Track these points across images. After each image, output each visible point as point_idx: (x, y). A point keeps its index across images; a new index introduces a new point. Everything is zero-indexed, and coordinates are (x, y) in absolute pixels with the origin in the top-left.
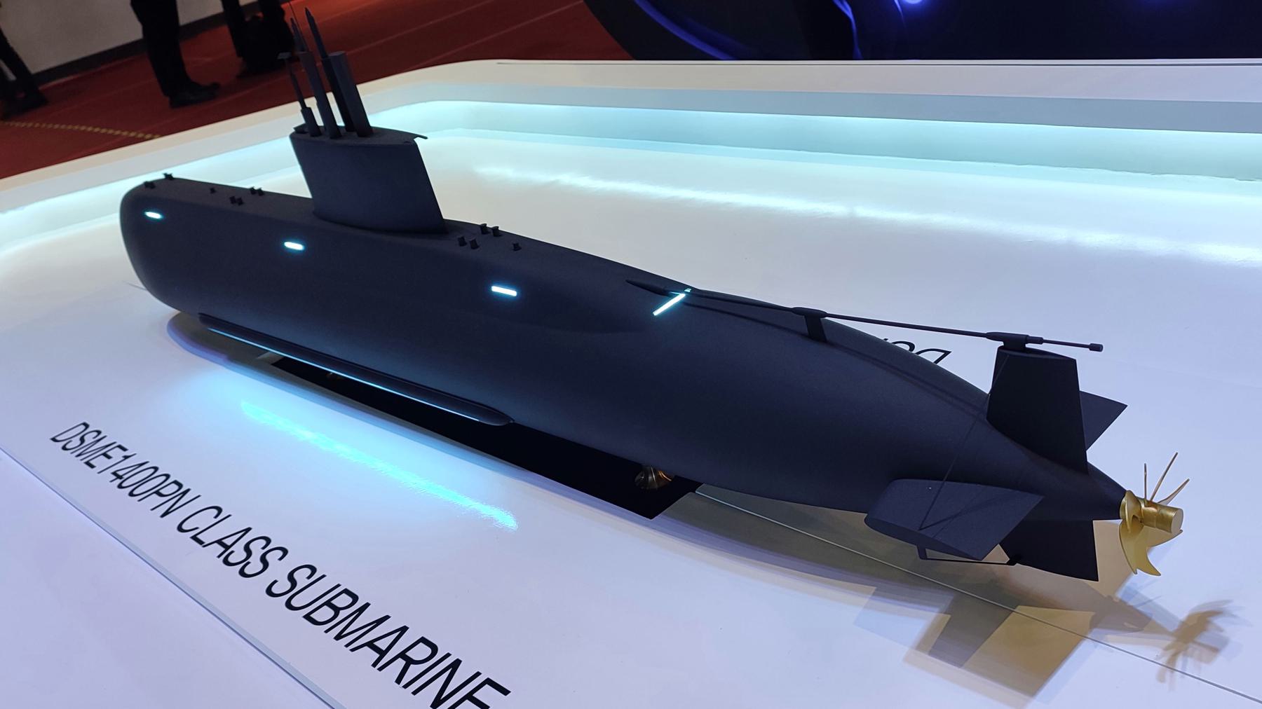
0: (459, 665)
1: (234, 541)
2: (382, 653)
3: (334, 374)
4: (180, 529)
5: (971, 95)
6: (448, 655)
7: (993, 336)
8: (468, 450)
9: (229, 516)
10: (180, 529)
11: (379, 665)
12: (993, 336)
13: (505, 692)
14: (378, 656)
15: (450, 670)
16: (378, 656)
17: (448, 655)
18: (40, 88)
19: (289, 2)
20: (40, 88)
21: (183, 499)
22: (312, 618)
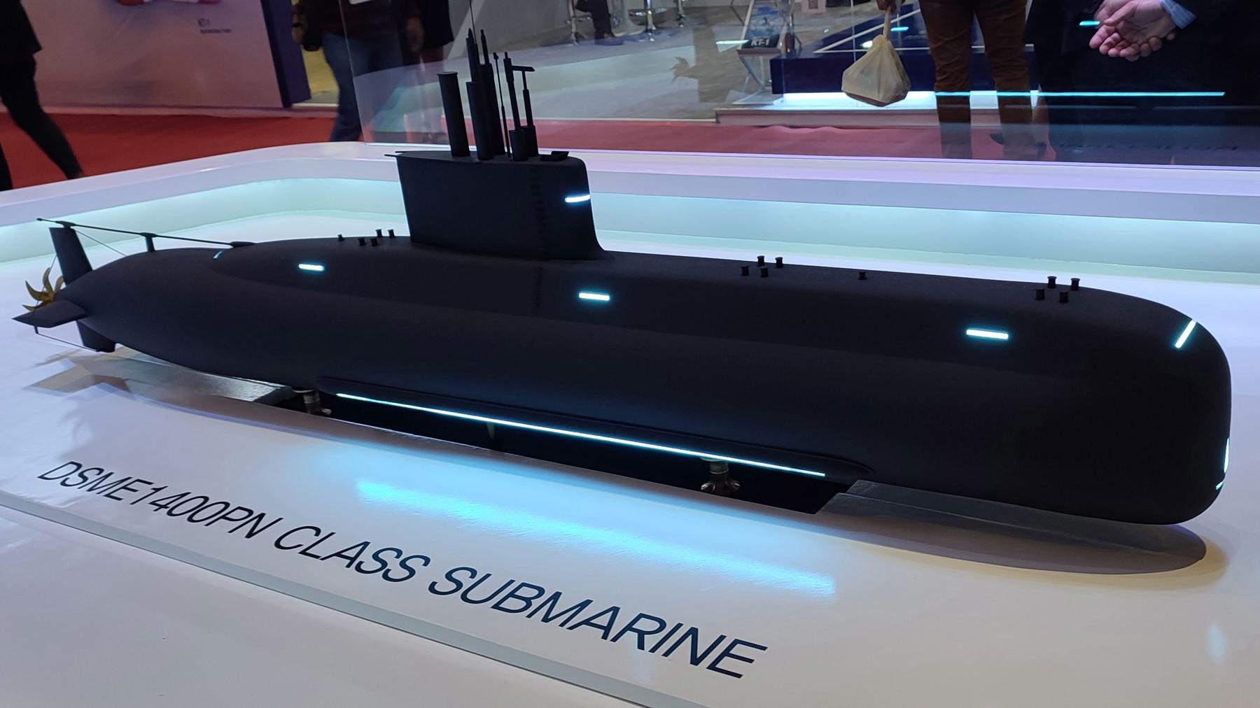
0: (559, 597)
1: (239, 525)
2: (607, 630)
3: (497, 426)
4: (278, 544)
5: (878, 249)
6: (679, 626)
7: (142, 234)
8: (773, 523)
9: (332, 534)
10: (278, 544)
11: (612, 635)
12: (142, 234)
13: (764, 648)
14: (646, 636)
15: (552, 601)
16: (646, 636)
17: (679, 626)
18: (717, 43)
19: (1107, 54)
20: (717, 43)
21: (104, 481)
22: (701, 656)
